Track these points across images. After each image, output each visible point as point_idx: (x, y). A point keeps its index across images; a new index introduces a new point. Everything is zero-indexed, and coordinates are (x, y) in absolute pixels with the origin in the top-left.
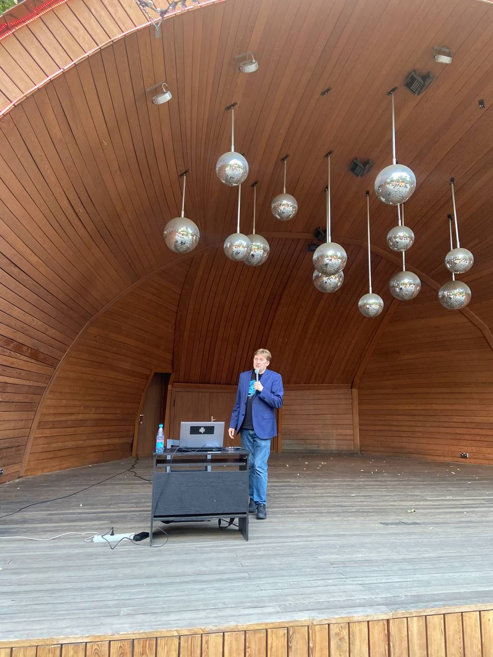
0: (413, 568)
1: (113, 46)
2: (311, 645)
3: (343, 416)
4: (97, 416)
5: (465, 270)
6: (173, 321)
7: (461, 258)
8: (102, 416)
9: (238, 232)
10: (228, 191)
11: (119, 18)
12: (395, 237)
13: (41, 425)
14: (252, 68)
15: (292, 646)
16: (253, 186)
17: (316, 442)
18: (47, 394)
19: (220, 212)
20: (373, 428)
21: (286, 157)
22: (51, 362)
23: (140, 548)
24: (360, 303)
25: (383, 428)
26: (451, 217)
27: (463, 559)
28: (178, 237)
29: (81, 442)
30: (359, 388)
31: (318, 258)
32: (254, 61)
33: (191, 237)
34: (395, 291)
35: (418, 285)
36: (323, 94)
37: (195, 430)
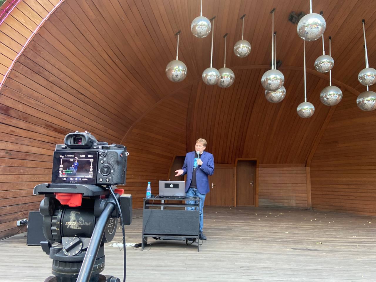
0: (292, 274)
16: (224, 37)
17: (282, 201)
20: (320, 193)
21: (244, 16)
23: (137, 251)
25: (328, 193)
27: (332, 272)
28: (174, 73)
30: (310, 167)
31: (264, 80)
34: (323, 100)
35: (339, 95)
37: (167, 186)
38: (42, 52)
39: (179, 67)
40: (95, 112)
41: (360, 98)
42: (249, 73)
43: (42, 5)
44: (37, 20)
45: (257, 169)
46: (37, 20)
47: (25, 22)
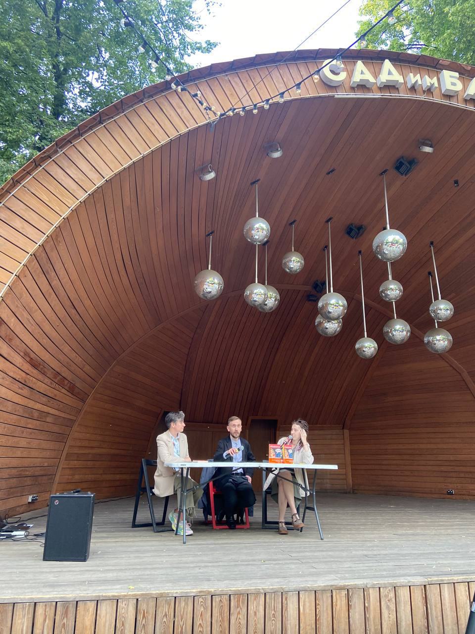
1: (180, 137)
2: (366, 605)
3: (336, 456)
7: (443, 309)
8: (117, 452)
11: (184, 117)
13: (69, 457)
18: (75, 427)
19: (239, 267)
21: (294, 221)
22: (81, 396)
24: (357, 346)
26: (431, 274)
31: (323, 306)
32: (279, 149)
33: (217, 286)
36: (328, 173)
38: (60, 244)
39: (214, 279)
40: (79, 336)
42: (302, 296)
43: (76, 180)
47: (48, 200)
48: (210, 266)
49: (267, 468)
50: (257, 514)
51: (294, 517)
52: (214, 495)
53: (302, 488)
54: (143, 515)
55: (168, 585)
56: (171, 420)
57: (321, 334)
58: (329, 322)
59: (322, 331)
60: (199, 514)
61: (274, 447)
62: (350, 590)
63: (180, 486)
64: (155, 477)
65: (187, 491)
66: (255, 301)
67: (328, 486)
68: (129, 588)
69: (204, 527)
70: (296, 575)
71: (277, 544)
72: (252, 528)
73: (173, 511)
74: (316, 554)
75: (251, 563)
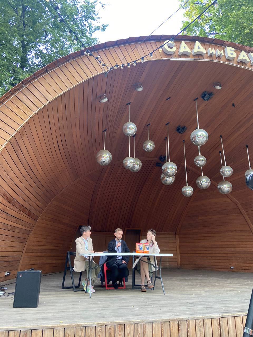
2: (188, 329)
4: (52, 248)
5: (229, 175)
6: (91, 199)
9: (129, 156)
10: (125, 137)
12: (198, 160)
13: (27, 251)
14: (140, 89)
15: (180, 330)
16: (167, 124)
18: (31, 234)
19: (120, 149)
21: (149, 124)
22: (35, 218)
24: (183, 190)
26: (221, 152)
29: (43, 261)
31: (164, 169)
32: (141, 87)
33: (108, 158)
36: (167, 99)
39: (107, 155)
40: (34, 185)
41: (220, 185)
42: (154, 163)
43: (33, 102)
44: (28, 112)
45: (141, 236)
46: (28, 112)
48: (105, 147)
49: (135, 256)
50: (130, 281)
51: (148, 282)
52: (106, 271)
53: (154, 266)
54: (68, 282)
55: (82, 320)
56: (84, 231)
57: (164, 184)
58: (168, 177)
59: (164, 182)
60: (98, 282)
61: (139, 244)
62: (180, 321)
63: (88, 266)
64: (74, 261)
65: (92, 269)
66: (129, 166)
67: (168, 265)
68: (60, 322)
69: (101, 288)
70: (150, 314)
71: (141, 297)
72: (127, 289)
73: (84, 280)
74: (161, 302)
75: (126, 307)
